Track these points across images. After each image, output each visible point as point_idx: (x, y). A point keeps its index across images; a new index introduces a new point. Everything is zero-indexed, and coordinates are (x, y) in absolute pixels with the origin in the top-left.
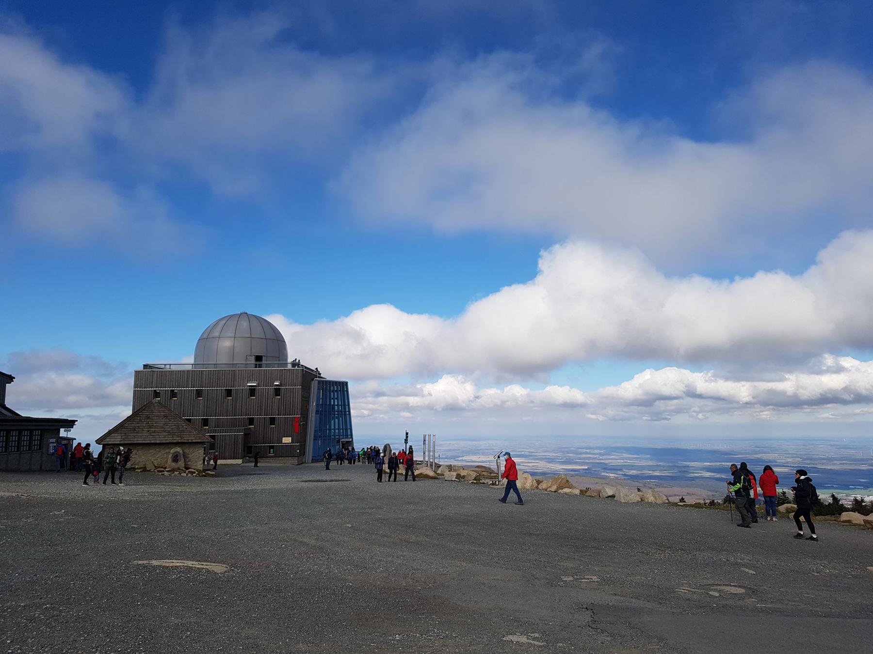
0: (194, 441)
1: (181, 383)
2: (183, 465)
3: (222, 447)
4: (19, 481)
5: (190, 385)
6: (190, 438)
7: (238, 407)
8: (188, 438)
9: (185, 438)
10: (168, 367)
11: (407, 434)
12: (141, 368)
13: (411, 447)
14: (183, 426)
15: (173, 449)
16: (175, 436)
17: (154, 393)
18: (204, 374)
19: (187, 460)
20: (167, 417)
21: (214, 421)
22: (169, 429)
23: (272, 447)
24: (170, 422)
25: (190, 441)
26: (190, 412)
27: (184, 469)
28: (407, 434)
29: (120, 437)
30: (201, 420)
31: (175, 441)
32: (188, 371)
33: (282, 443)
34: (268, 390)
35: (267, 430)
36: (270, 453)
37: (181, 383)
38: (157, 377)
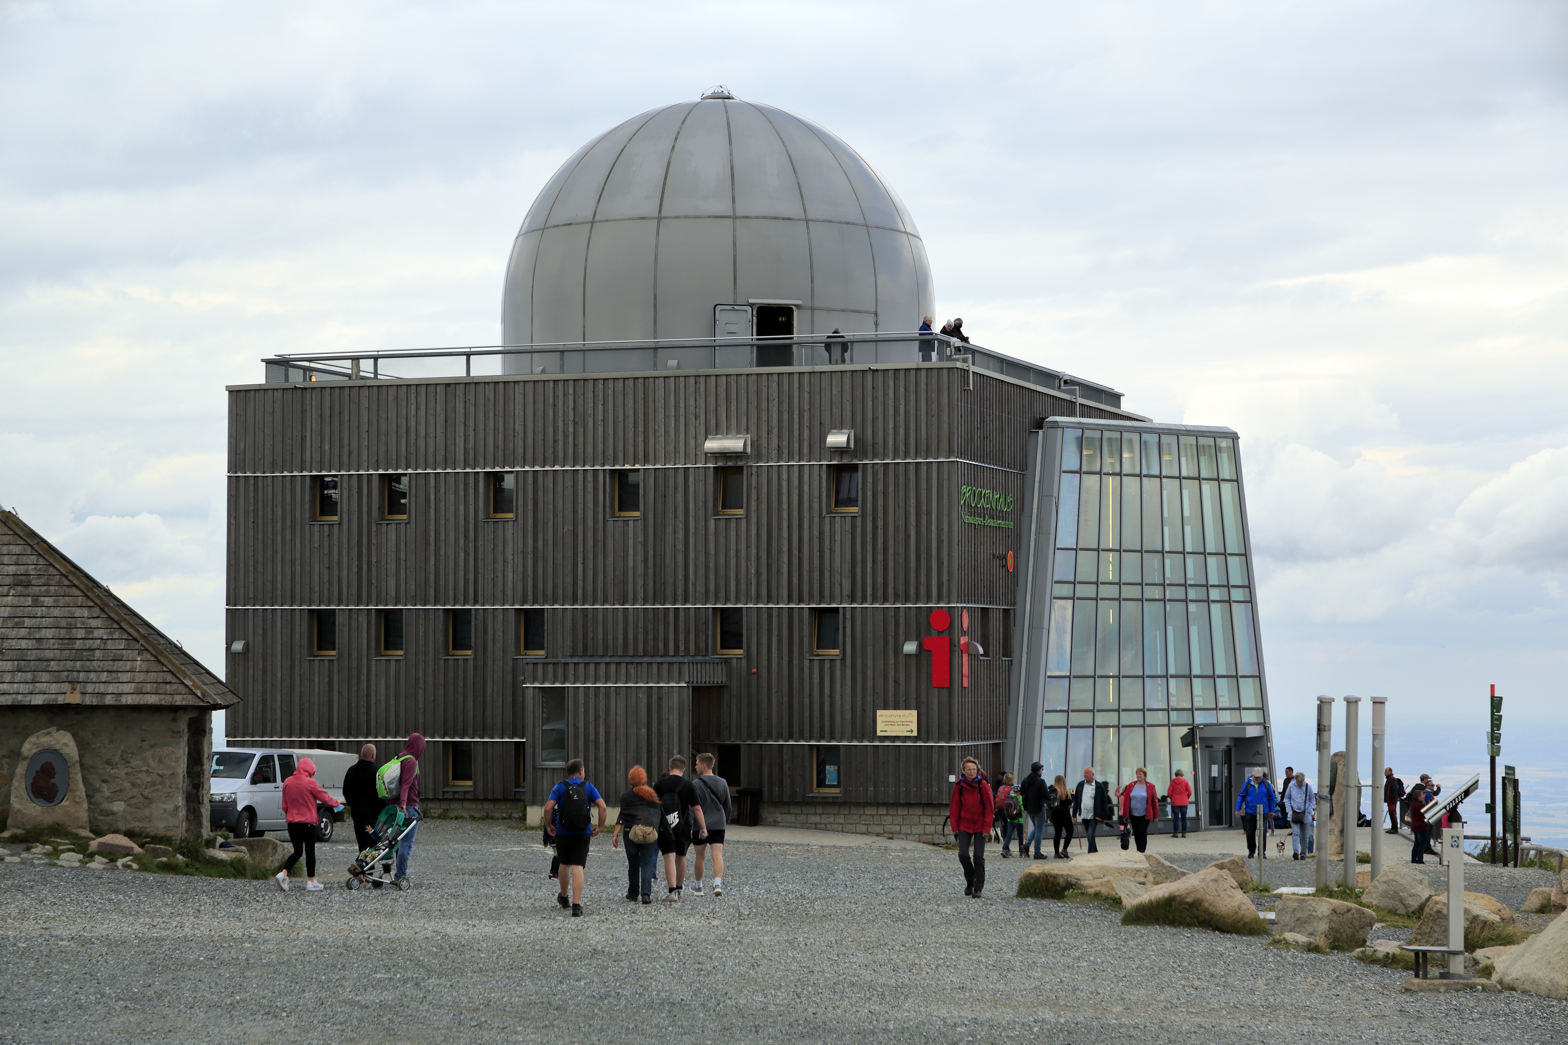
0: (128, 700)
1: (422, 443)
2: (82, 812)
3: (597, 748)
4: (239, 901)
5: (461, 457)
6: (111, 688)
7: (669, 558)
8: (102, 688)
9: (90, 688)
10: (366, 366)
11: (1496, 704)
12: (257, 376)
13: (1510, 770)
14: (90, 629)
15: (32, 739)
16: (45, 677)
17: (312, 488)
18: (519, 398)
19: (106, 791)
20: (28, 585)
21: (569, 622)
22: (24, 644)
23: (826, 756)
24: (39, 611)
25: (109, 700)
26: (466, 580)
27: (85, 833)
28: (1496, 704)
29: (1131, 738)
30: (512, 617)
31: (38, 700)
32: (448, 385)
33: (874, 736)
34: (875, 474)
35: (801, 669)
36: (821, 783)
37: (422, 443)
38: (321, 416)
